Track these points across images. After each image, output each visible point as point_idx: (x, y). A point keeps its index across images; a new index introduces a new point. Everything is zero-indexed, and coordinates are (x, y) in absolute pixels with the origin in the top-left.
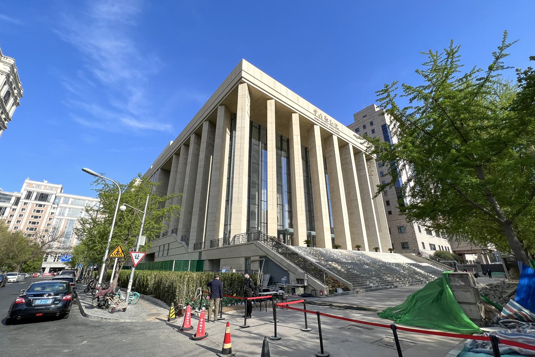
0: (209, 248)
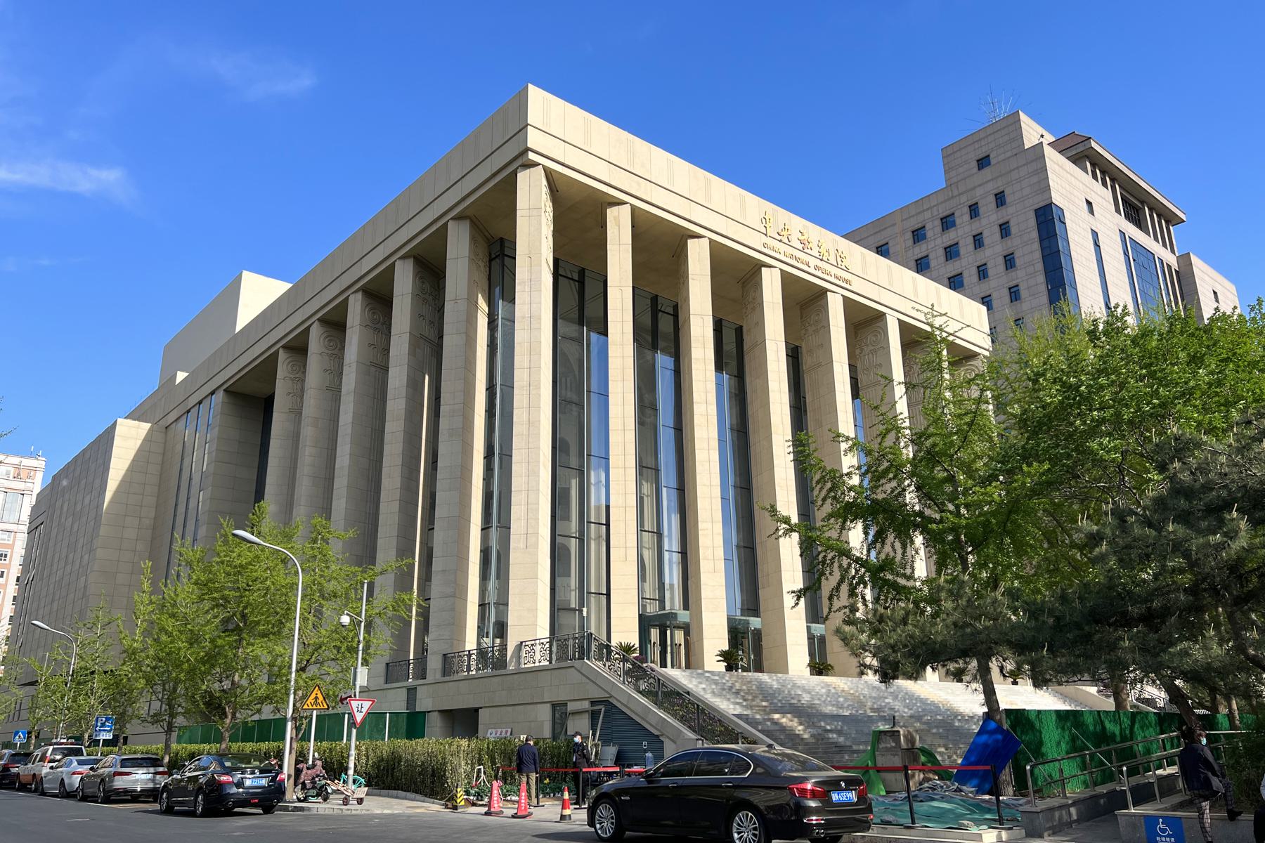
0: (438, 676)
